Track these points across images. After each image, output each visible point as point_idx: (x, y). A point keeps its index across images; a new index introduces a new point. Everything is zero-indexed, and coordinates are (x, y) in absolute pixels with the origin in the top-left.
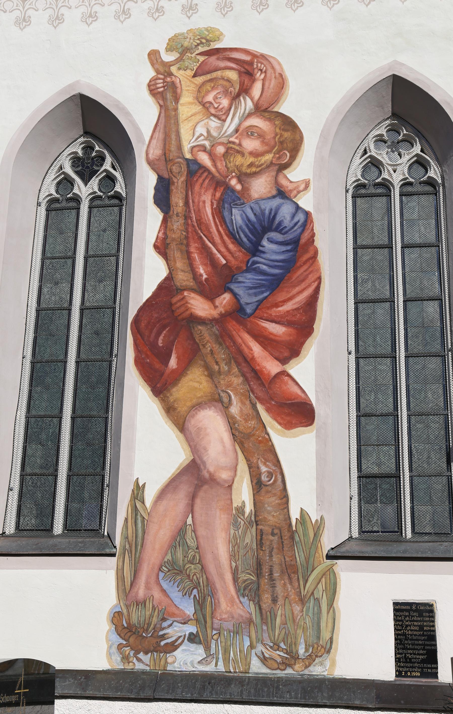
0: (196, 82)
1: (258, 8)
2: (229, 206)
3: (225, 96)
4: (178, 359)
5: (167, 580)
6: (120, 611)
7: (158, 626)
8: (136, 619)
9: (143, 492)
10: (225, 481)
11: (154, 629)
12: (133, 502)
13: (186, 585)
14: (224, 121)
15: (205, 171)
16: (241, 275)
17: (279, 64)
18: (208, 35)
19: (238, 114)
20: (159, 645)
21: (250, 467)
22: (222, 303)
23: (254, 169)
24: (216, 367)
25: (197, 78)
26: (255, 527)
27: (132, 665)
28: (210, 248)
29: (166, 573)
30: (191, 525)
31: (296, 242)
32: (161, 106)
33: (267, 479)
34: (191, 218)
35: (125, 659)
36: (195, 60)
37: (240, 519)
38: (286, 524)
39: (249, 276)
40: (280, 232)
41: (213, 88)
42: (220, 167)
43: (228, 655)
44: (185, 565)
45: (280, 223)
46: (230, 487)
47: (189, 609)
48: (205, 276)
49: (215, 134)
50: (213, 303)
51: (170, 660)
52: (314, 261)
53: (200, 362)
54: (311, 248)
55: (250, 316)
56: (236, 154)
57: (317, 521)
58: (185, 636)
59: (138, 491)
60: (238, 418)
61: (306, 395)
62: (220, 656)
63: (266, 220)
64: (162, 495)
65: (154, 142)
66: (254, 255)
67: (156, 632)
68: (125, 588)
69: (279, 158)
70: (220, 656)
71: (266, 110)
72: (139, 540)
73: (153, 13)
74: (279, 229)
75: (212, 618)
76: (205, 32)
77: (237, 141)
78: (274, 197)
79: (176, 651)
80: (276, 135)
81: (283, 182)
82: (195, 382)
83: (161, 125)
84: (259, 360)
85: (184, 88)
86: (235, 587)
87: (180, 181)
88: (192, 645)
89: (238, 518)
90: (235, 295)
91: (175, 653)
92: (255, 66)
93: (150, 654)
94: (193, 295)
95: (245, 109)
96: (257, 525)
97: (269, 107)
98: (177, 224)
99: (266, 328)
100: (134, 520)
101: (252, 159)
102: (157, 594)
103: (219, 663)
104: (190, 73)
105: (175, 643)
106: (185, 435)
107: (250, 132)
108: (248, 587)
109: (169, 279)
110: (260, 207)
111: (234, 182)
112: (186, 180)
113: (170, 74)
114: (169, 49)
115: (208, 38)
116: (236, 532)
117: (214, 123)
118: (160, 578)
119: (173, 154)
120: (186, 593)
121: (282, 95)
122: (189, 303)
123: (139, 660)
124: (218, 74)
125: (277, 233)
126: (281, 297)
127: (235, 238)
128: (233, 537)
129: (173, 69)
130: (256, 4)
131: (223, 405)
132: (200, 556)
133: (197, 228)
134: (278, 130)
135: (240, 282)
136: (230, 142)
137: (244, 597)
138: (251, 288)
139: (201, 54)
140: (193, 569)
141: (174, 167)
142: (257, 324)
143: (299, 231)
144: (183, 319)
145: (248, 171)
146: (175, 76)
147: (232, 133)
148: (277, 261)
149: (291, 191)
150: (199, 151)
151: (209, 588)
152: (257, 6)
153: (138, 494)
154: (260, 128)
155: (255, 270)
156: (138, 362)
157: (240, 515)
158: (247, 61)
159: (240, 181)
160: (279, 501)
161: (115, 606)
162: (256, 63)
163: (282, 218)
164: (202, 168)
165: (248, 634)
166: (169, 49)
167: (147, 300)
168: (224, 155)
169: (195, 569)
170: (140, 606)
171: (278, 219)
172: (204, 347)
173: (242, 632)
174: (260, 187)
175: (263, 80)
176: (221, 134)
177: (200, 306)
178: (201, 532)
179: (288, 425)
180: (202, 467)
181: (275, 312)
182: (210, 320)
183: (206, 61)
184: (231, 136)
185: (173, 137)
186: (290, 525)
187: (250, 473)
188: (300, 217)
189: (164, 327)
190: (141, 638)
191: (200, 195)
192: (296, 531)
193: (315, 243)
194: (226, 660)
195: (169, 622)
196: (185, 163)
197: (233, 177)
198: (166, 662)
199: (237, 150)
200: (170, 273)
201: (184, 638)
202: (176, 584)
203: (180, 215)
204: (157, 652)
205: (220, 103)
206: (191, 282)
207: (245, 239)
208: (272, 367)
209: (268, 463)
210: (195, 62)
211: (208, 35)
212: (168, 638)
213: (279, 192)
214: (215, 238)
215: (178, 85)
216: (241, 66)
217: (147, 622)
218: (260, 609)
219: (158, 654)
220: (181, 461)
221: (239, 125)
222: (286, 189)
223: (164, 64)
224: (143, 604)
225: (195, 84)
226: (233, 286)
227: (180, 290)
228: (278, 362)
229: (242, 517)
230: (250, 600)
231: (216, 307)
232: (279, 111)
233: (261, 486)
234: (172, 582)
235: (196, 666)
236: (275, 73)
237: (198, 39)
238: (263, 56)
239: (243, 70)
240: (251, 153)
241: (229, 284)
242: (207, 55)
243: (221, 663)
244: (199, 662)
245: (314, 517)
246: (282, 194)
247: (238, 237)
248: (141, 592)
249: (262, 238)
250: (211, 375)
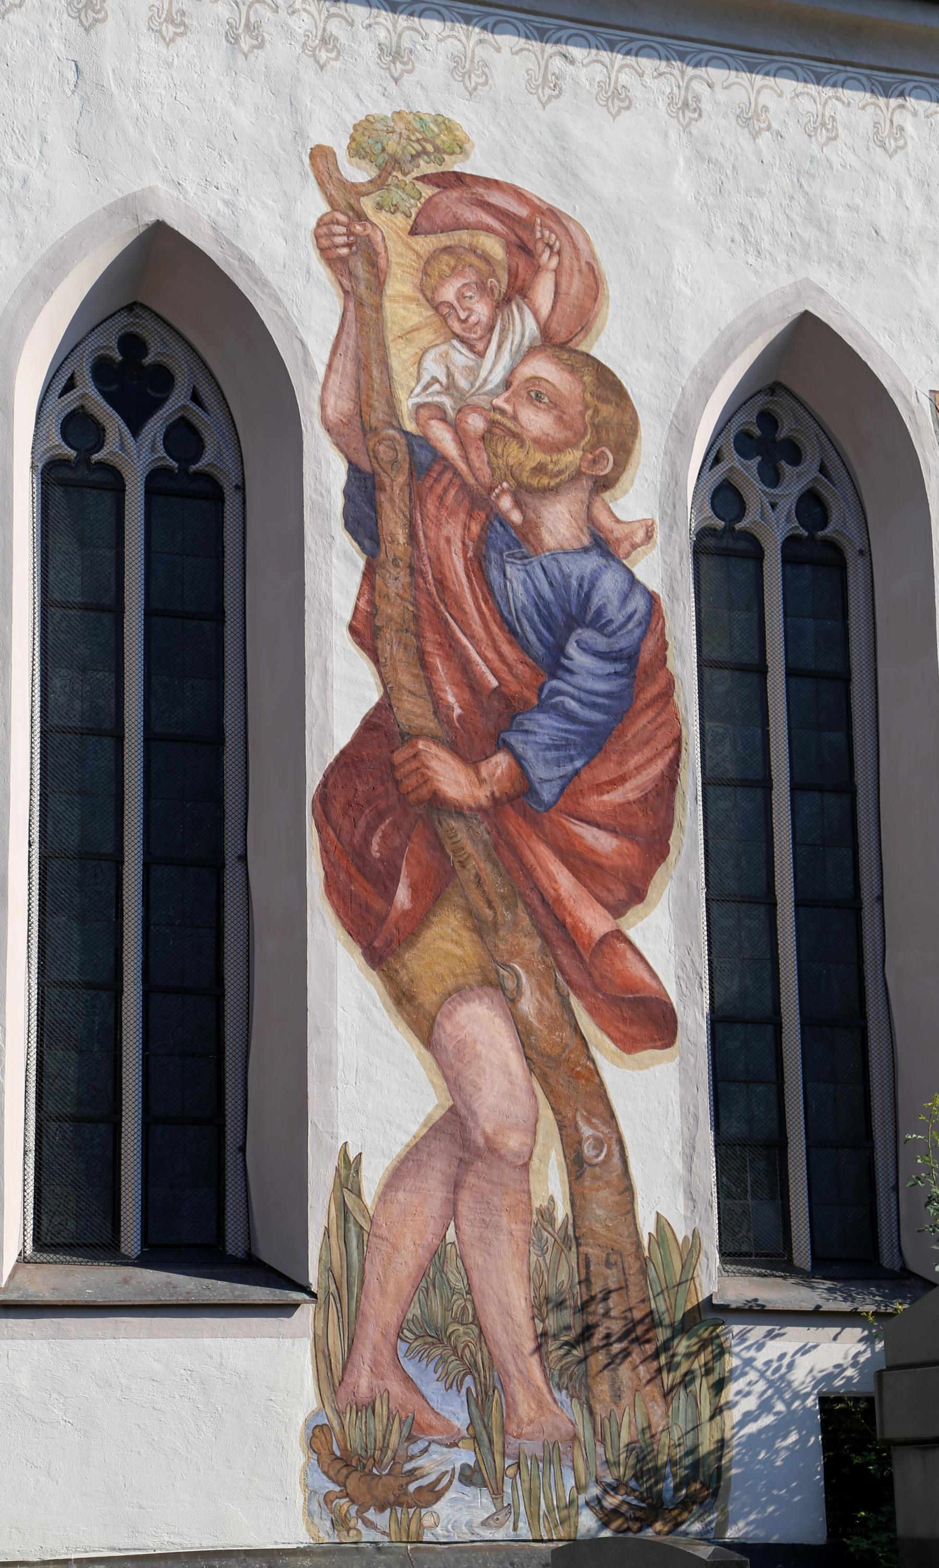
0: (417, 248)
1: (540, 90)
2: (498, 557)
3: (481, 296)
4: (413, 890)
5: (413, 1358)
6: (325, 1425)
7: (401, 1452)
8: (358, 1440)
9: (357, 1172)
10: (518, 1155)
11: (394, 1459)
12: (339, 1194)
13: (451, 1367)
14: (481, 355)
15: (446, 468)
16: (528, 715)
17: (588, 240)
18: (438, 135)
19: (507, 346)
20: (406, 1493)
21: (561, 1127)
22: (494, 775)
23: (545, 481)
24: (488, 912)
25: (420, 239)
26: (574, 1249)
27: (357, 1535)
28: (464, 647)
29: (411, 1344)
30: (454, 1243)
31: (630, 657)
32: (346, 292)
33: (592, 1153)
34: (422, 574)
35: (340, 1522)
36: (412, 195)
37: (546, 1233)
38: (632, 1244)
40: (601, 630)
41: (454, 272)
42: (477, 465)
43: (537, 1507)
44: (445, 1329)
45: (599, 613)
46: (526, 1166)
47: (456, 1412)
48: (457, 711)
49: (463, 383)
50: (477, 772)
51: (428, 1521)
52: (668, 702)
53: (456, 899)
54: (662, 674)
55: (548, 808)
56: (507, 439)
57: (686, 1238)
58: (454, 1469)
59: (349, 1170)
60: (535, 1023)
61: (660, 983)
62: (522, 1508)
63: (574, 600)
64: (397, 1176)
65: (335, 379)
66: (553, 676)
67: (398, 1466)
68: (332, 1375)
69: (594, 462)
70: (522, 1508)
71: (563, 346)
72: (355, 1274)
73: (314, 49)
74: (599, 623)
75: (504, 1432)
76: (432, 126)
77: (508, 408)
78: (585, 550)
79: (439, 1503)
80: (587, 407)
81: (604, 519)
82: (446, 942)
83: (349, 341)
84: (570, 904)
85: (393, 258)
86: (544, 1371)
87: (396, 483)
88: (467, 1489)
89: (543, 1230)
90: (518, 759)
91: (436, 1507)
92: (538, 235)
93: (389, 1510)
94: (434, 749)
95: (523, 336)
96: (578, 1245)
97: (571, 340)
98: (395, 581)
99: (580, 836)
100: (341, 1232)
101: (539, 457)
102: (395, 1387)
103: (521, 1524)
105: (436, 1487)
106: (434, 1055)
107: (536, 393)
108: (567, 1369)
109: (384, 708)
110: (561, 570)
111: (506, 503)
112: (409, 485)
113: (361, 217)
114: (357, 151)
115: (438, 142)
116: (541, 1259)
117: (461, 357)
118: (400, 1355)
119: (378, 416)
120: (452, 1384)
121: (596, 315)
122: (428, 768)
123: (368, 1524)
124: (464, 237)
125: (595, 632)
126: (605, 771)
127: (513, 632)
128: (535, 1269)
129: (367, 205)
130: (536, 81)
131: (504, 994)
132: (474, 1309)
133: (437, 600)
134: (588, 397)
135: (527, 732)
136: (495, 408)
137: (560, 1390)
138: (548, 748)
139: (424, 178)
140: (463, 1334)
141: (381, 448)
142: (564, 827)
143: (638, 632)
144: (419, 802)
145: (534, 482)
146: (372, 224)
147: (497, 386)
148: (597, 694)
149: (618, 541)
150: (431, 418)
151: (496, 1374)
152: (537, 87)
153: (348, 1176)
154: (554, 386)
155: (555, 707)
156: (332, 886)
157: (545, 1224)
158: (521, 218)
159: (518, 504)
160: (617, 1198)
161: (316, 1414)
162: (538, 228)
163: (605, 600)
164: (439, 457)
165: (571, 1464)
166: (357, 151)
167: (343, 752)
168: (483, 438)
169: (466, 1334)
170: (364, 1412)
171: (596, 601)
172: (464, 867)
173: (560, 1460)
175: (555, 271)
176: (477, 385)
177: (452, 779)
179: (628, 1044)
180: (471, 1124)
181: (594, 803)
182: (470, 808)
183: (436, 199)
184: (494, 394)
185: (595, 699)
186: (639, 1245)
187: (562, 1139)
188: (638, 603)
189: (380, 816)
190: (369, 1478)
191: (439, 525)
192: (650, 1258)
193: (669, 665)
194: (533, 1517)
195: (421, 1445)
196: (403, 441)
197: (503, 491)
198: (420, 1525)
199: (509, 430)
200: (386, 695)
201: (453, 1476)
202: (431, 1366)
203: (401, 564)
204: (401, 1505)
205: (471, 311)
206: (431, 721)
207: (532, 638)
208: (594, 921)
209: (594, 1120)
210: (413, 198)
211: (438, 135)
212: (422, 1477)
213: (595, 540)
214: (474, 626)
215: (380, 249)
216: (508, 227)
217: (379, 1445)
218: (591, 1413)
219: (404, 1510)
220: (429, 1109)
221: (512, 372)
222: (610, 536)
223: (344, 184)
224: (370, 1410)
225: (417, 253)
226: (515, 739)
227: (408, 737)
228: (606, 912)
229: (550, 1229)
230: (572, 1397)
231: (482, 781)
232: (592, 353)
233: (582, 1167)
234: (424, 1362)
235: (477, 1530)
236: (578, 260)
237: (418, 141)
238: (553, 214)
239: (513, 238)
240: (536, 441)
241: (506, 734)
242: (438, 186)
243: (523, 1525)
244: (483, 1524)
245: (681, 1232)
246: (602, 544)
247: (519, 630)
248: (363, 1382)
249: (567, 640)
250: (481, 929)
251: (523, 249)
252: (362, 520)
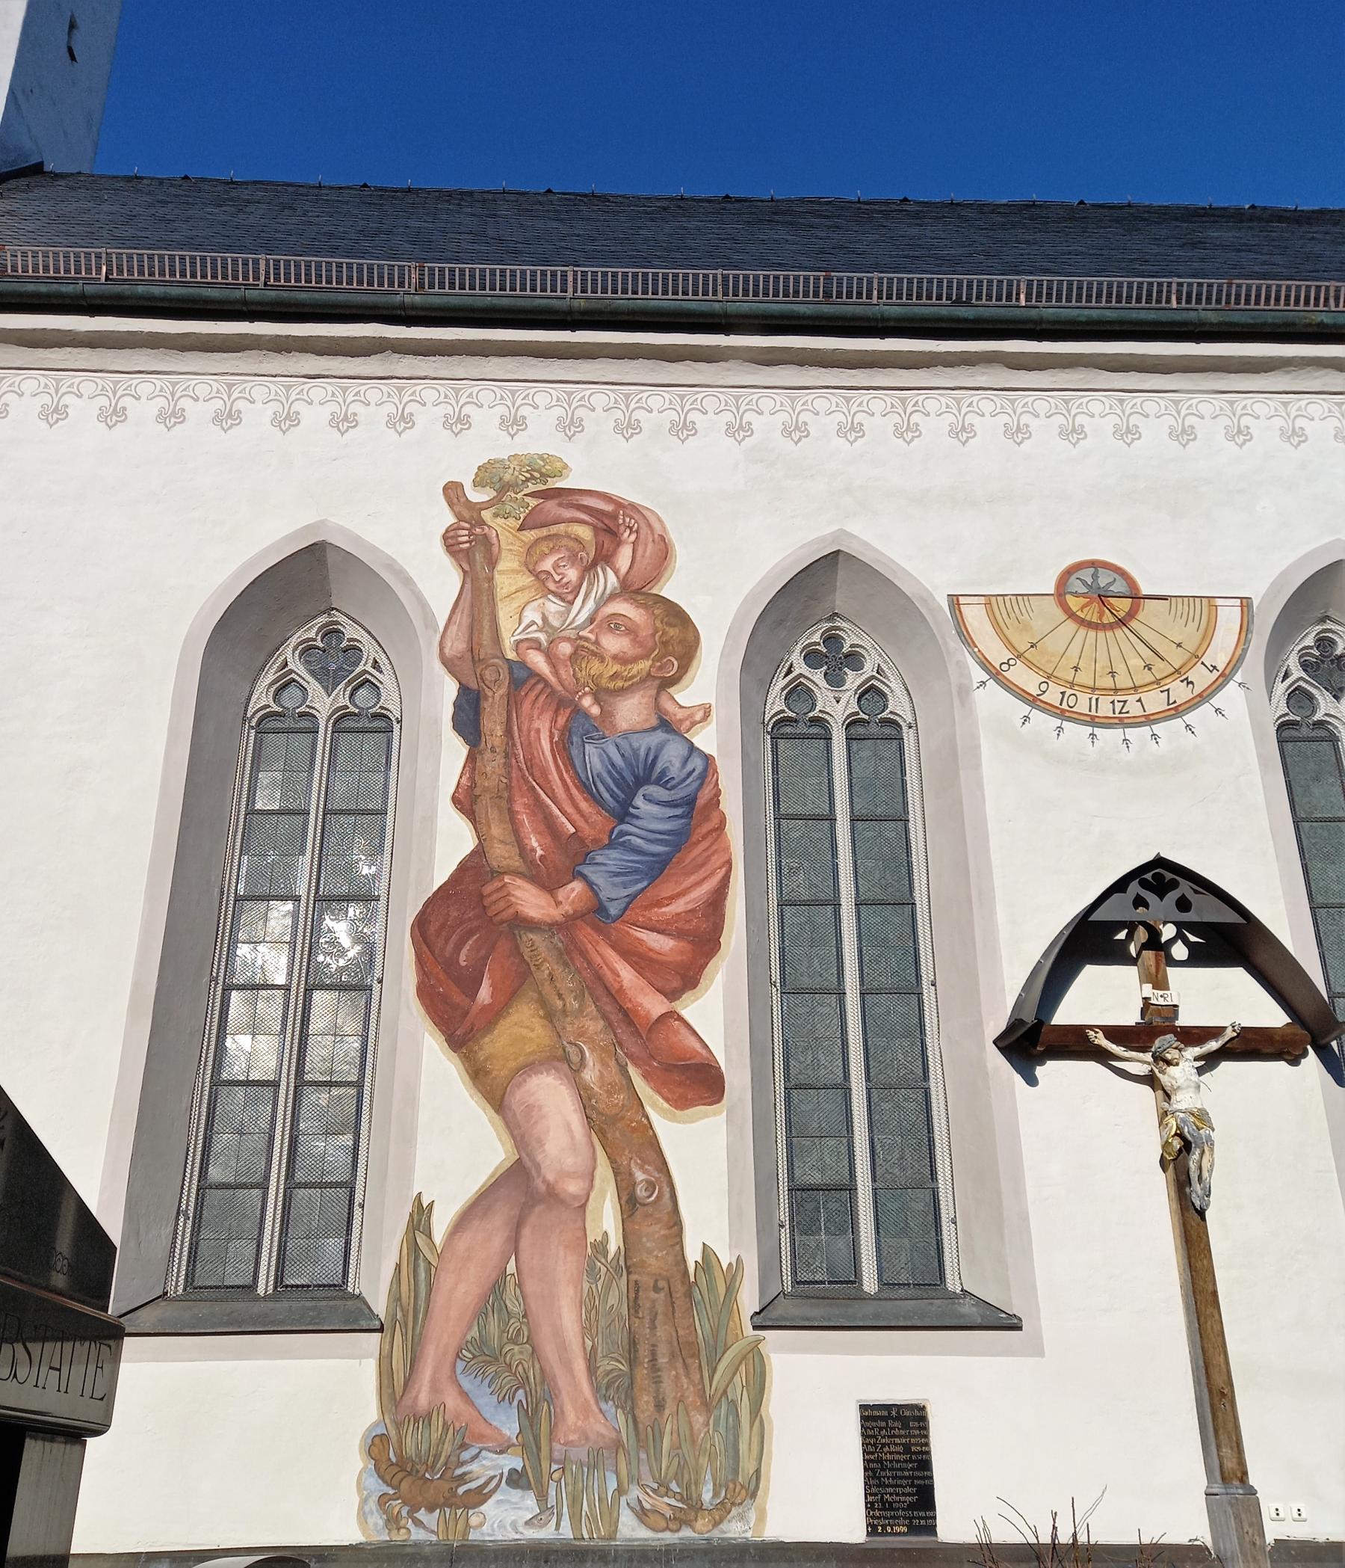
39: (614, 854)
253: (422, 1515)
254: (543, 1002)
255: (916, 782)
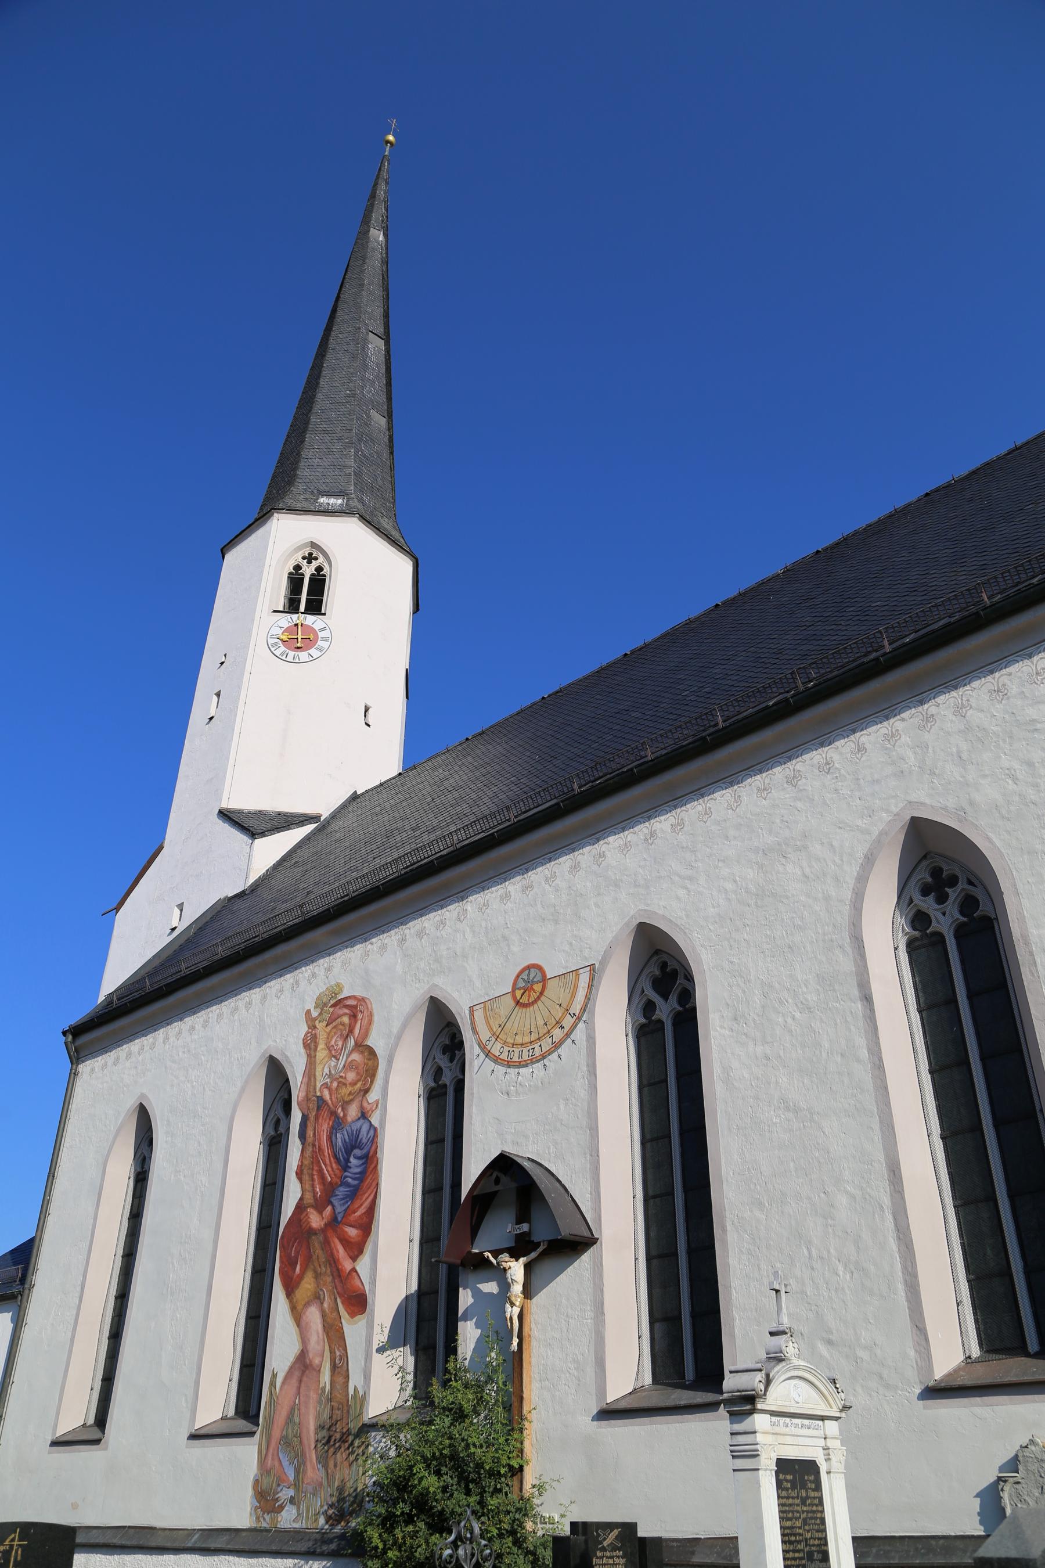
39: (341, 1189)
84: (341, 1260)
98: (309, 1150)
104: (325, 1023)
164: (324, 1102)
174: (353, 1112)
178: (303, 1410)
251: (354, 1017)
252: (302, 1136)
253: (265, 1515)
254: (315, 1271)
255: (915, 1030)
